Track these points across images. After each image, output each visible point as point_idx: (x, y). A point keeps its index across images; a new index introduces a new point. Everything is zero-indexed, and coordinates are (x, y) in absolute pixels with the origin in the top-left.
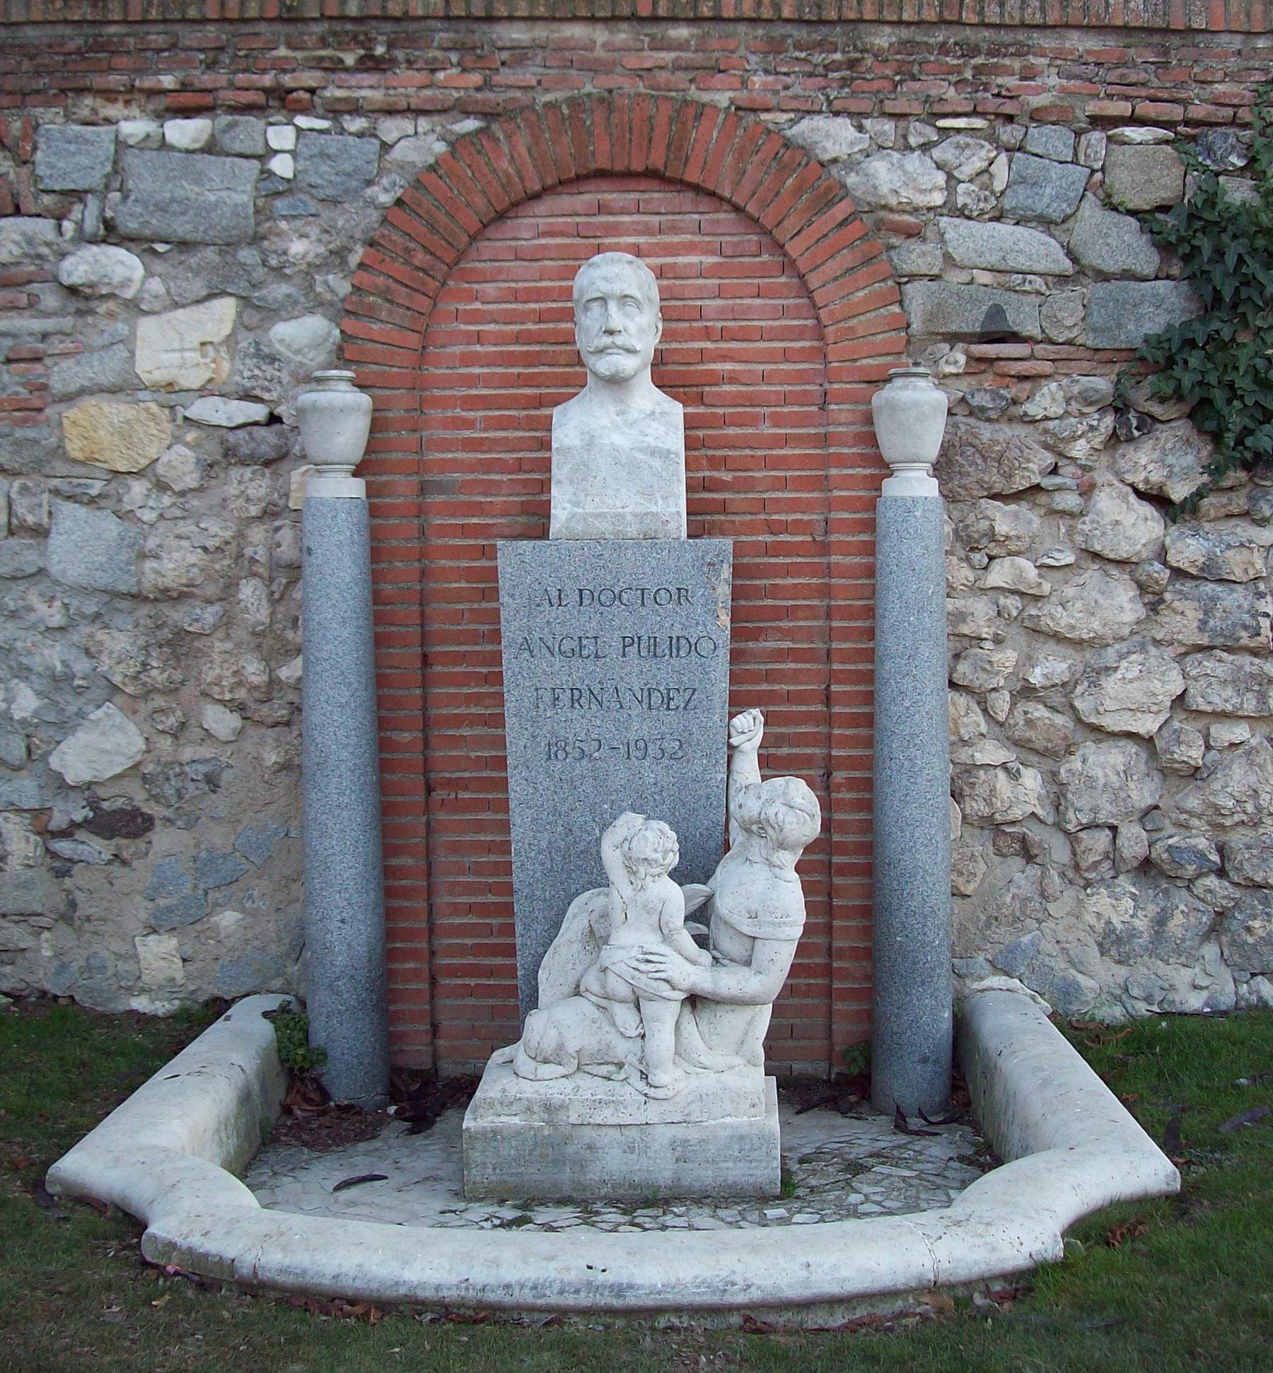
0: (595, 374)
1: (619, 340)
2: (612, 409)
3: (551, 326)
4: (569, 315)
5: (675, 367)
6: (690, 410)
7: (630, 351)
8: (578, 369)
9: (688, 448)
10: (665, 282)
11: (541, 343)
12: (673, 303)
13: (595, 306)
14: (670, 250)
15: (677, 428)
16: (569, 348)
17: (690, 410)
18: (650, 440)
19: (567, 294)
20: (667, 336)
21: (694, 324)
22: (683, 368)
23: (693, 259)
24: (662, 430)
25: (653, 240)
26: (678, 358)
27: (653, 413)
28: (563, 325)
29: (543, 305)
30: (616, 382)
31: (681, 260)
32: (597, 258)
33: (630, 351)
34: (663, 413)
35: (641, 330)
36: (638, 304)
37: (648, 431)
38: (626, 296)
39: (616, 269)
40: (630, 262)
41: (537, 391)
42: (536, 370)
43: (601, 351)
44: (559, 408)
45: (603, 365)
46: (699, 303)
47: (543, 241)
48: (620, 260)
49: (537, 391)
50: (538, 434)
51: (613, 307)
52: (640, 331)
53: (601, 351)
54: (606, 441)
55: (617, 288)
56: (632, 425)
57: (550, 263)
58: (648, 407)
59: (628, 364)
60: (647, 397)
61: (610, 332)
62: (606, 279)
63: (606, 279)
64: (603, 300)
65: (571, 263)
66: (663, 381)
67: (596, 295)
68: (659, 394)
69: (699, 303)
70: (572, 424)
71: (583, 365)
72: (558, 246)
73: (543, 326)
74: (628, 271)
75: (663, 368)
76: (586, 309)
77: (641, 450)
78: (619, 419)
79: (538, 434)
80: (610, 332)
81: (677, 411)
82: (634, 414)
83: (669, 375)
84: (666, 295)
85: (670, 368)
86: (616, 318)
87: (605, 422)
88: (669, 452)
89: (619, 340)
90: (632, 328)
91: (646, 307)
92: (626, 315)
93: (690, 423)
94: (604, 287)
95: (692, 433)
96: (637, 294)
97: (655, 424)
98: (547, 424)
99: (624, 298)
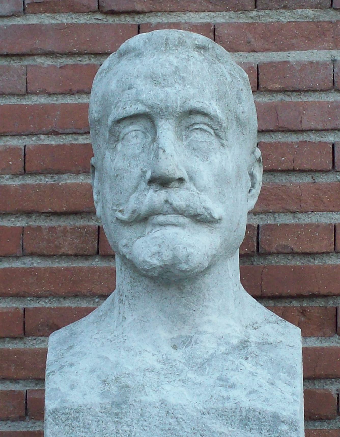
0: (131, 265)
1: (179, 197)
2: (163, 334)
3: (47, 180)
4: (83, 160)
5: (283, 261)
6: (313, 343)
7: (201, 219)
8: (98, 263)
9: (310, 417)
10: (265, 99)
11: (28, 213)
12: (280, 138)
13: (133, 131)
14: (275, 38)
15: (290, 372)
16: (80, 222)
17: (313, 343)
18: (240, 397)
19: (80, 122)
20: (268, 201)
21: (322, 179)
22: (298, 262)
23: (320, 55)
24: (263, 375)
25: (243, 19)
26: (290, 242)
27: (244, 344)
28: (68, 180)
29: (31, 142)
30: (173, 281)
31: (296, 56)
32: (136, 41)
33: (201, 219)
34: (264, 344)
35: (222, 179)
36: (217, 130)
37: (235, 377)
38: (193, 112)
39: (172, 60)
40: (201, 48)
41: (18, 305)
42: (17, 264)
43: (143, 219)
44: (62, 333)
45: (147, 247)
46: (331, 138)
47: (33, 20)
48: (181, 43)
49: (18, 305)
50: (18, 387)
51: (167, 131)
52: (221, 179)
53: (143, 219)
54: (153, 398)
55: (176, 95)
56: (201, 366)
57: (47, 62)
58: (236, 333)
59: (194, 244)
60: (231, 312)
61: (161, 182)
62: (154, 79)
63: (154, 79)
64: (147, 118)
65: (86, 61)
66: (266, 289)
67: (133, 109)
68: (258, 311)
69: (331, 138)
70: (84, 364)
71: (111, 256)
72: (61, 28)
73: (30, 181)
74: (197, 64)
75: (259, 262)
76: (115, 138)
77: (221, 414)
78: (177, 355)
79: (18, 387)
80: (161, 182)
81: (289, 341)
82: (207, 346)
83: (270, 270)
84: (269, 126)
85: (273, 261)
86: (174, 153)
87: (150, 359)
88: (276, 417)
89: (179, 197)
90: (205, 172)
91: (232, 134)
92: (194, 149)
93: (315, 370)
94: (149, 94)
95: (318, 386)
96: (214, 108)
97: (248, 365)
98: (35, 369)
99: (189, 117)
